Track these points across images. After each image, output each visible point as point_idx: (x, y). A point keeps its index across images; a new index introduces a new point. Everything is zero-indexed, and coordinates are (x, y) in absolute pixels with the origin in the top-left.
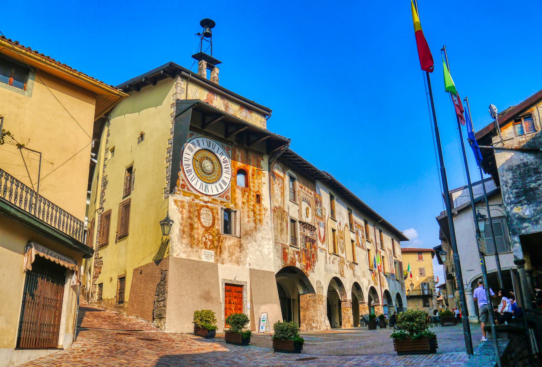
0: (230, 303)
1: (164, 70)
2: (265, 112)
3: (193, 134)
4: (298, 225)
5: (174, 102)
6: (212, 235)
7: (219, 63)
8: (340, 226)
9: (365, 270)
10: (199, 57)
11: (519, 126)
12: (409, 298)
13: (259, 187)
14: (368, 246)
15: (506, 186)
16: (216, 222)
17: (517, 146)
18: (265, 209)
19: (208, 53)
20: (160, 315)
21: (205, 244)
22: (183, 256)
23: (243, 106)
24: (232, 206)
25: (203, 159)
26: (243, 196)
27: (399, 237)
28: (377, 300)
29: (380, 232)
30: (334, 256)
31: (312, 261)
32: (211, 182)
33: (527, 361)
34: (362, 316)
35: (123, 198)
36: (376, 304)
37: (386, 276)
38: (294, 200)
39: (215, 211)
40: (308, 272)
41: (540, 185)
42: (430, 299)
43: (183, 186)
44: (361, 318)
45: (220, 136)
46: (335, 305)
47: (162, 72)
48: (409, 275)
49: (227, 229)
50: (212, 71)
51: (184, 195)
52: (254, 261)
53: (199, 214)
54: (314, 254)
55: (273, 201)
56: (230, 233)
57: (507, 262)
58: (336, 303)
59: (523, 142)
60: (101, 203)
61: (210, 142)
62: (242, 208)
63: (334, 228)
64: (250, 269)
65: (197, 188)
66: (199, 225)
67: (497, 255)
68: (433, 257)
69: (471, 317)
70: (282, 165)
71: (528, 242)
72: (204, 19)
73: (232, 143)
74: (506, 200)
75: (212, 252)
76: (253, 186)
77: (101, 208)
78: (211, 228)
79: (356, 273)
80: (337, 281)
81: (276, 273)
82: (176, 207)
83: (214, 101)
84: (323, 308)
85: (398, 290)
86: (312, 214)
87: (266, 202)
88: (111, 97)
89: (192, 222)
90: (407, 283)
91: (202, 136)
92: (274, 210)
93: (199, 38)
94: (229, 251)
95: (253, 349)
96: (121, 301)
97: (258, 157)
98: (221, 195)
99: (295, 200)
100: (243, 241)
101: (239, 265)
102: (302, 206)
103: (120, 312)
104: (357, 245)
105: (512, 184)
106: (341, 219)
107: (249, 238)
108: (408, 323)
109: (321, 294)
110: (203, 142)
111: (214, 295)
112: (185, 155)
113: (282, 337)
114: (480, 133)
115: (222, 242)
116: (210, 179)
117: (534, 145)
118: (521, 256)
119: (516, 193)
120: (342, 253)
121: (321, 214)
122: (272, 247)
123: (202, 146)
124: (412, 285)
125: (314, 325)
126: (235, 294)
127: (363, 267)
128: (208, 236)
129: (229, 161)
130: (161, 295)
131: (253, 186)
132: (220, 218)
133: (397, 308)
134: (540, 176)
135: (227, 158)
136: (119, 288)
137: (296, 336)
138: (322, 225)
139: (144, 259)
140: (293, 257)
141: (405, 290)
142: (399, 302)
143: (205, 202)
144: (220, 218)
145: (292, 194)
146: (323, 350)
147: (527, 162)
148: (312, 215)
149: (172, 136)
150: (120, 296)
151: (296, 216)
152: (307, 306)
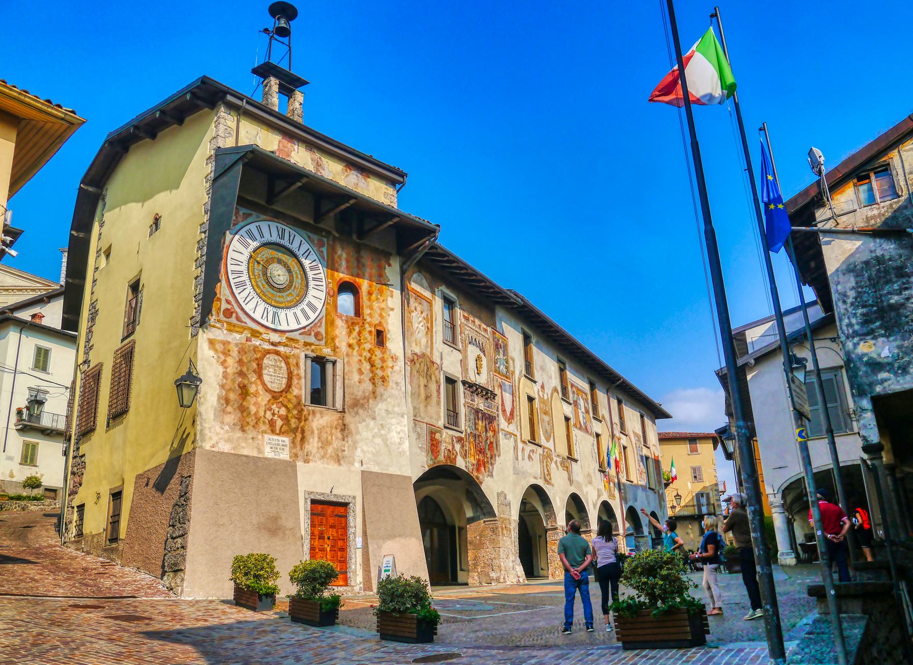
0: (321, 537)
1: (193, 94)
3: (250, 215)
4: (461, 388)
5: (213, 152)
6: (286, 407)
7: (305, 83)
10: (265, 71)
11: (865, 187)
13: (381, 315)
14: (597, 427)
15: (844, 302)
16: (295, 381)
17: (862, 225)
18: (394, 358)
19: (284, 66)
20: (175, 564)
21: (272, 423)
22: (225, 448)
23: (351, 165)
24: (326, 351)
26: (350, 333)
27: (654, 411)
29: (620, 402)
31: (489, 455)
33: (899, 654)
35: (123, 340)
38: (452, 342)
39: (292, 361)
40: (481, 477)
41: (908, 299)
43: (228, 313)
45: (304, 219)
47: (188, 97)
49: (318, 397)
50: (290, 97)
52: (370, 456)
53: (260, 367)
54: (491, 443)
55: (410, 343)
57: (851, 451)
59: (874, 217)
60: (86, 353)
62: (348, 355)
63: (532, 395)
65: (257, 316)
67: (830, 432)
68: (715, 448)
69: (783, 554)
70: (428, 276)
71: (885, 407)
72: (271, 3)
74: (845, 328)
75: (286, 440)
76: (370, 315)
77: (85, 362)
80: (537, 494)
81: (414, 480)
82: (212, 353)
83: (293, 154)
84: (510, 543)
85: (653, 506)
87: (395, 344)
88: (48, 126)
89: (246, 382)
90: (669, 494)
91: (268, 218)
92: (412, 361)
93: (266, 38)
94: (319, 438)
95: (341, 633)
99: (454, 341)
100: (348, 418)
101: (340, 464)
103: (112, 560)
104: (575, 425)
105: (856, 298)
106: (545, 377)
107: (361, 411)
108: (644, 580)
110: (271, 230)
111: (288, 523)
112: (231, 254)
113: (394, 610)
114: (794, 201)
115: (306, 420)
116: (281, 300)
117: (895, 223)
118: (874, 437)
119: (863, 315)
120: (548, 440)
121: (507, 368)
122: (406, 429)
124: (678, 497)
125: (493, 575)
126: (331, 521)
128: (277, 410)
129: (322, 272)
130: (178, 525)
131: (370, 315)
132: (303, 374)
133: (653, 539)
134: (908, 282)
136: (111, 514)
137: (423, 607)
138: (508, 388)
140: (450, 448)
141: (665, 506)
144: (303, 374)
145: (449, 332)
146: (480, 634)
147: (883, 255)
148: (489, 370)
149: (206, 218)
150: (113, 528)
151: (456, 372)
152: (480, 540)
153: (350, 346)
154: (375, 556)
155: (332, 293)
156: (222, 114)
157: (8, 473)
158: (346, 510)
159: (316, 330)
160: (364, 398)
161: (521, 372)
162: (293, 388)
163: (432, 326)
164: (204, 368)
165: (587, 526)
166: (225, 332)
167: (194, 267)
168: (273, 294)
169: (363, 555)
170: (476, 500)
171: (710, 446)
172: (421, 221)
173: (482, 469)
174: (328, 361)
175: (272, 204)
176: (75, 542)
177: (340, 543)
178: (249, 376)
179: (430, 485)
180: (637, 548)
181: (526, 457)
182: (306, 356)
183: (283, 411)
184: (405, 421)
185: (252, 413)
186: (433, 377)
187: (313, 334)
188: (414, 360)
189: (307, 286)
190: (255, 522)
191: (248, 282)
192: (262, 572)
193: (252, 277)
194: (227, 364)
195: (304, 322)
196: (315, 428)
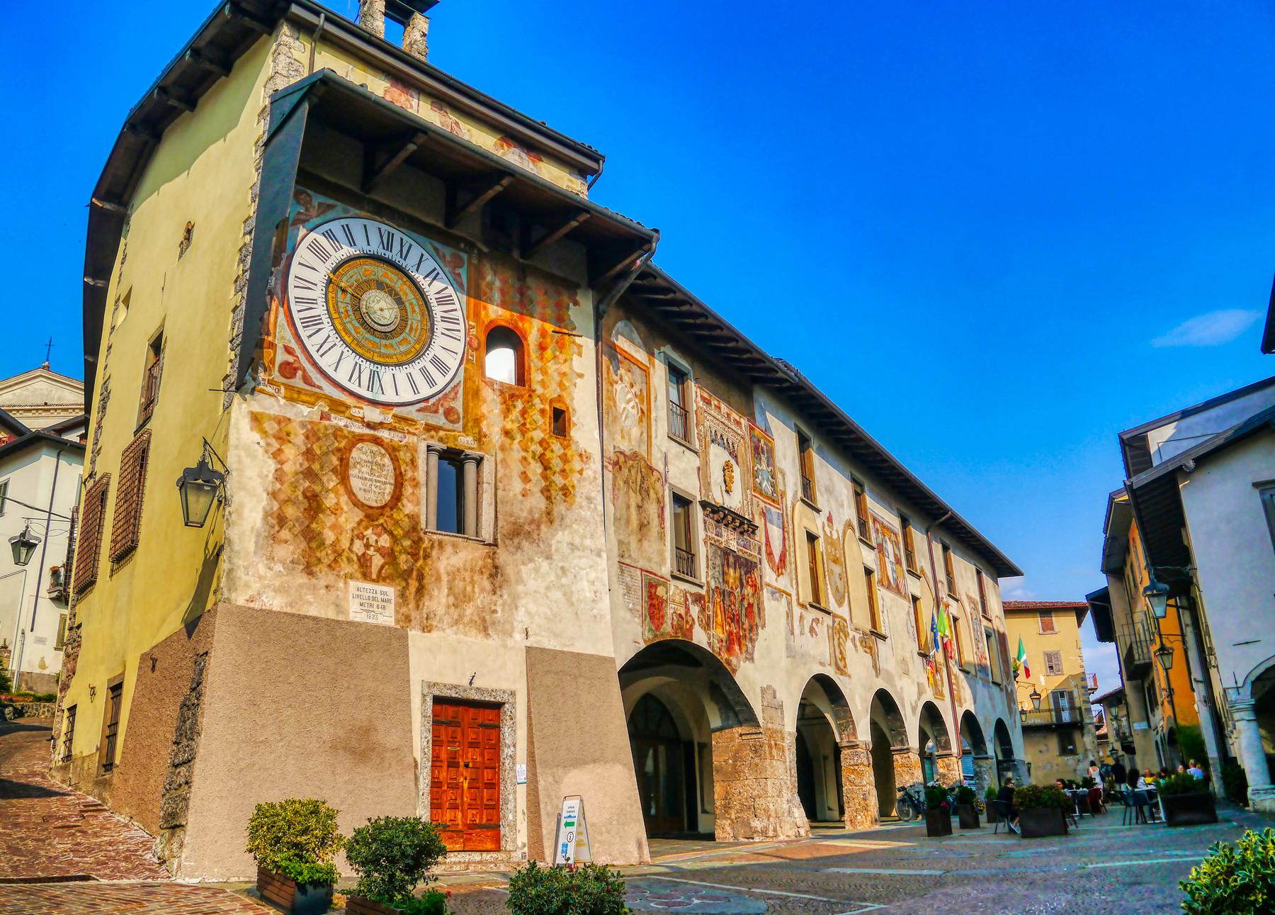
0: (453, 764)
2: (584, 162)
3: (330, 207)
4: (699, 514)
5: (267, 101)
6: (391, 533)
8: (831, 527)
9: (908, 655)
12: (1028, 730)
13: (561, 384)
14: (914, 586)
16: (408, 490)
21: (364, 562)
22: (275, 603)
24: (465, 442)
25: (364, 286)
26: (507, 412)
27: (995, 564)
28: (943, 739)
30: (813, 614)
31: (746, 626)
32: (394, 360)
34: (903, 789)
36: (941, 752)
37: (966, 672)
38: (683, 437)
39: (404, 456)
40: (734, 661)
42: (1077, 736)
43: (289, 370)
44: (899, 795)
46: (825, 758)
48: (1021, 672)
51: (290, 399)
53: (344, 463)
54: (750, 605)
55: (611, 434)
56: (460, 529)
58: (830, 752)
61: (391, 236)
62: (503, 449)
63: (814, 531)
64: (529, 649)
65: (341, 377)
66: (344, 499)
69: (1256, 792)
70: (642, 328)
73: (470, 246)
75: (390, 591)
78: (387, 512)
79: (882, 664)
80: (825, 687)
81: (620, 664)
82: (256, 436)
84: (782, 771)
85: (1001, 712)
86: (743, 480)
87: (584, 432)
89: (317, 488)
91: (363, 214)
92: (616, 463)
94: (450, 589)
96: (108, 766)
97: (559, 294)
98: (427, 406)
99: (686, 436)
100: (503, 556)
102: (711, 457)
104: (881, 582)
106: (833, 502)
107: (525, 544)
109: (776, 727)
110: (368, 234)
111: (388, 737)
115: (427, 556)
116: (390, 351)
120: (840, 604)
121: (773, 485)
123: (361, 247)
125: (757, 824)
127: (900, 646)
128: (374, 538)
129: (459, 302)
131: (542, 383)
133: (999, 763)
135: (450, 291)
138: (775, 517)
139: (164, 620)
140: (682, 611)
142: (1001, 744)
143: (369, 425)
144: (421, 475)
145: (678, 422)
148: (745, 488)
149: (254, 207)
151: (691, 487)
152: (734, 766)
153: (507, 433)
154: (549, 796)
155: (475, 344)
156: (284, 38)
157: (37, 662)
158: (498, 715)
159: (446, 405)
160: (532, 522)
161: (796, 493)
162: (405, 501)
163: (649, 410)
164: (240, 461)
165: (902, 742)
166: (282, 401)
167: (233, 292)
168: (374, 343)
169: (528, 794)
170: (725, 697)
171: (1072, 619)
172: (628, 222)
173: (737, 648)
174: (467, 457)
175: (368, 192)
176: (61, 767)
177: (487, 774)
178: (325, 479)
179: (651, 675)
180: (978, 775)
181: (807, 630)
182: (429, 449)
183: (385, 541)
184: (603, 562)
185: (328, 542)
186: (652, 492)
187: (441, 410)
188: (619, 463)
189: (432, 332)
190: (326, 737)
191: (325, 319)
192: (302, 839)
193: (335, 316)
194: (283, 457)
195: (426, 391)
196: (442, 571)
